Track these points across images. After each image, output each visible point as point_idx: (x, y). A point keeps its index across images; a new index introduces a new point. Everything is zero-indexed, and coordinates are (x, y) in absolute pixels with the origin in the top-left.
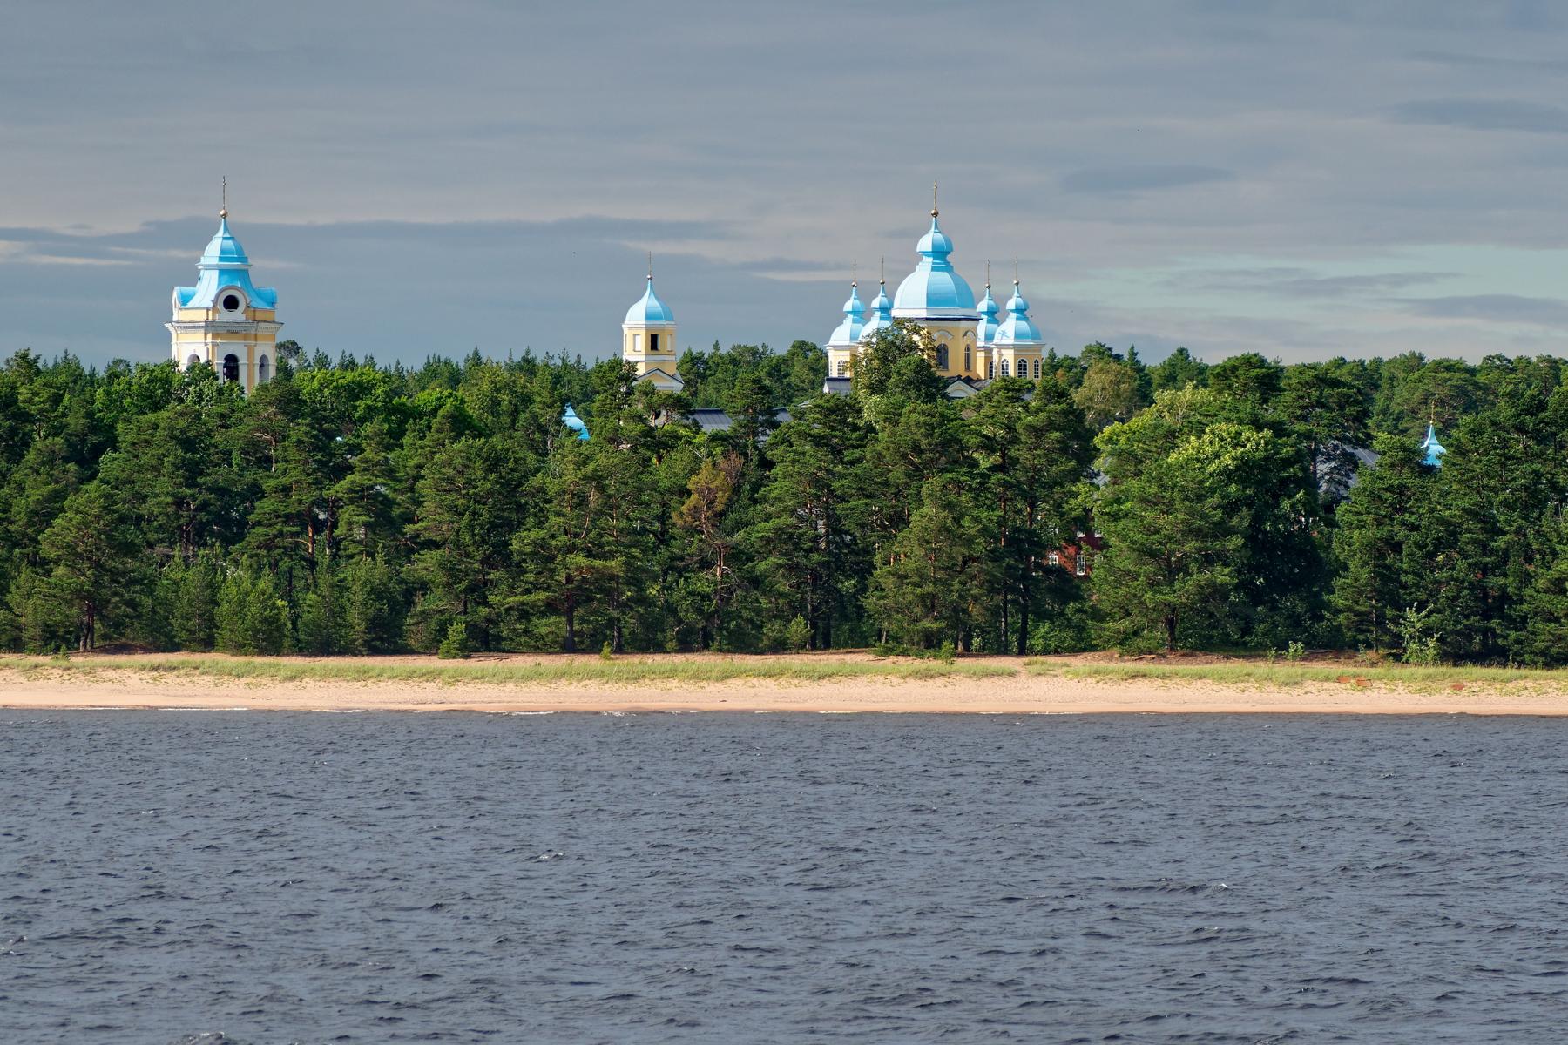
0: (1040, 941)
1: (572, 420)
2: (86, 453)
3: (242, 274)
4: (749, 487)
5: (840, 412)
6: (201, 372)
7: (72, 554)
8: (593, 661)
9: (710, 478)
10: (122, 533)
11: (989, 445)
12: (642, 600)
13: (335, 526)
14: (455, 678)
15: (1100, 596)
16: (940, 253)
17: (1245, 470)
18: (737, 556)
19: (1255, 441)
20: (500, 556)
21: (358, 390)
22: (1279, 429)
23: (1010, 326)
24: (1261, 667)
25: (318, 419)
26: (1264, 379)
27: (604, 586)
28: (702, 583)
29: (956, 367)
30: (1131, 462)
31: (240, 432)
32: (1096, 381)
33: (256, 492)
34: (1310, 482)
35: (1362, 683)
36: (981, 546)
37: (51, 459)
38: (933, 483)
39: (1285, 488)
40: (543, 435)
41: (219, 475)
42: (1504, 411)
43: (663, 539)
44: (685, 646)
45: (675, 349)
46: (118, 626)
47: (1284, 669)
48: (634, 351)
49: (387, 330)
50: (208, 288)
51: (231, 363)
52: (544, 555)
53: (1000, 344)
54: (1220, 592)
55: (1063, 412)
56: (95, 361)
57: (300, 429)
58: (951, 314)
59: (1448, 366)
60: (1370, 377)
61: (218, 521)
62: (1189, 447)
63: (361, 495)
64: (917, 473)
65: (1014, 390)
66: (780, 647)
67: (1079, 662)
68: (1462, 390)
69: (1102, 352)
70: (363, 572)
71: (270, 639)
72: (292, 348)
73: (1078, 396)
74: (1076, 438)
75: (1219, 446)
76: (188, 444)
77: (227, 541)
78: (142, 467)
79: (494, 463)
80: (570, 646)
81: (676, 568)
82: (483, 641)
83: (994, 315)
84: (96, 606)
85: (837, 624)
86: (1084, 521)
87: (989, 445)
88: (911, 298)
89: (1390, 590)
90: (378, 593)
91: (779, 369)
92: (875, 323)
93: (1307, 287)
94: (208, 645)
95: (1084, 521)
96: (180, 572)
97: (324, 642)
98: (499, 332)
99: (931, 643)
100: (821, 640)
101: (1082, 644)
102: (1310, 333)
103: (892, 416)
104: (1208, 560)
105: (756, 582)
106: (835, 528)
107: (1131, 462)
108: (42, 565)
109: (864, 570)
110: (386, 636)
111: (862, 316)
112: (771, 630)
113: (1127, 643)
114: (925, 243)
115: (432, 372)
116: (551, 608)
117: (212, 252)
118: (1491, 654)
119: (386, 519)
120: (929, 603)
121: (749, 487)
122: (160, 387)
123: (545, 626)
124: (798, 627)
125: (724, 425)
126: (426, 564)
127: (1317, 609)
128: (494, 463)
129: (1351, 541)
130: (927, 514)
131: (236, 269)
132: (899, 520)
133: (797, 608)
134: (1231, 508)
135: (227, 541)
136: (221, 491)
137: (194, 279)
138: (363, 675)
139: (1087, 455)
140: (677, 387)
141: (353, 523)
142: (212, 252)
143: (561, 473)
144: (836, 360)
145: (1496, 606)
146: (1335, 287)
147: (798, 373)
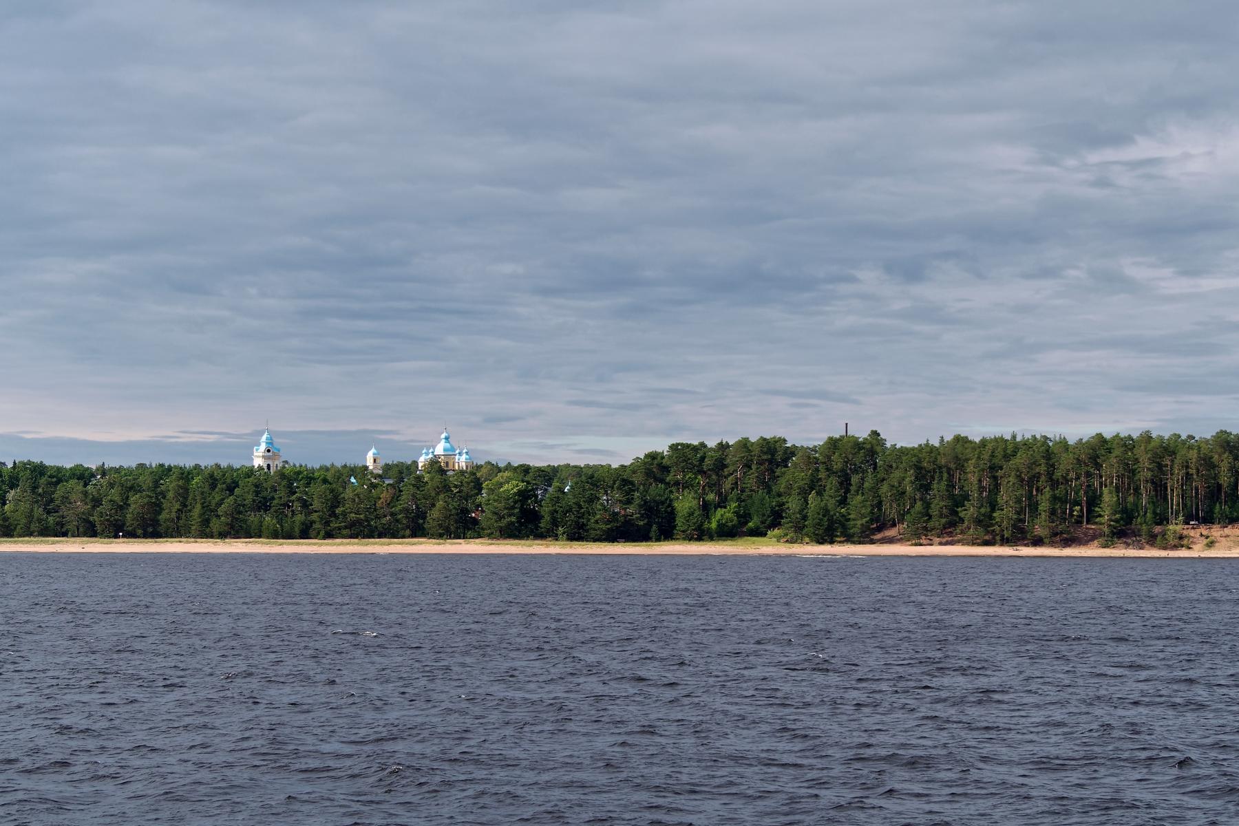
0: (1133, 659)
1: (353, 480)
2: (231, 489)
3: (271, 443)
4: (396, 497)
5: (419, 478)
6: (260, 468)
7: (226, 514)
8: (356, 540)
9: (385, 495)
10: (238, 509)
11: (456, 486)
12: (369, 525)
13: (1101, 477)
14: (321, 545)
15: (484, 524)
16: (447, 438)
17: (520, 493)
18: (392, 514)
19: (522, 485)
20: (334, 514)
21: (299, 473)
22: (528, 483)
23: (464, 457)
24: (523, 542)
25: (289, 480)
26: (526, 469)
27: (359, 522)
28: (384, 521)
29: (451, 467)
30: (491, 491)
31: (270, 484)
32: (484, 471)
33: (273, 498)
34: (536, 496)
35: (547, 546)
36: (454, 512)
37: (222, 490)
38: (442, 496)
39: (529, 497)
40: (345, 484)
41: (264, 494)
42: (583, 478)
43: (375, 510)
44: (379, 537)
45: (381, 463)
46: (237, 532)
47: (528, 542)
48: (370, 463)
49: (311, 459)
50: (263, 447)
51: (269, 466)
52: (344, 514)
53: (461, 462)
54: (512, 523)
55: (474, 479)
56: (237, 465)
57: (284, 483)
58: (449, 454)
59: (576, 467)
60: (555, 470)
61: (263, 505)
62: (506, 487)
63: (299, 499)
64: (438, 494)
65: (462, 472)
66: (403, 537)
67: (477, 541)
68: (578, 471)
69: (489, 463)
70: (300, 518)
71: (275, 535)
72: (286, 462)
73: (478, 475)
74: (478, 486)
75: (512, 487)
76: (257, 486)
77: (266, 511)
78: (245, 493)
79: (332, 491)
80: (351, 537)
81: (378, 517)
82: (329, 535)
83: (460, 454)
84: (232, 527)
85: (418, 531)
86: (480, 505)
87: (456, 486)
88: (440, 450)
89: (555, 523)
90: (303, 524)
91: (408, 467)
92: (431, 456)
93: (546, 447)
94: (260, 537)
95: (480, 505)
96: (253, 518)
97: (289, 536)
98: (339, 460)
99: (440, 536)
100: (414, 535)
101: (479, 537)
102: (539, 459)
103: (432, 479)
104: (510, 515)
105: (397, 521)
106: (417, 507)
107: (491, 491)
108: (218, 516)
109: (424, 518)
110: (305, 534)
111: (427, 454)
112: (401, 533)
113: (490, 536)
114: (443, 436)
115: (321, 468)
116: (346, 527)
117: (264, 438)
118: (579, 538)
119: (305, 505)
120: (440, 526)
121: (396, 497)
122: (250, 472)
123: (345, 532)
124: (408, 532)
125: (391, 482)
126: (315, 516)
127: (537, 527)
128: (332, 491)
129: (545, 510)
130: (440, 504)
131: (270, 442)
132: (433, 505)
133: (408, 527)
134: (515, 502)
135: (266, 511)
136: (265, 498)
137: (259, 445)
138: (298, 544)
139: (480, 489)
140: (380, 472)
141: (297, 506)
142: (264, 438)
143: (348, 494)
144: (420, 465)
145: (582, 526)
146: (552, 447)
147: (413, 468)
